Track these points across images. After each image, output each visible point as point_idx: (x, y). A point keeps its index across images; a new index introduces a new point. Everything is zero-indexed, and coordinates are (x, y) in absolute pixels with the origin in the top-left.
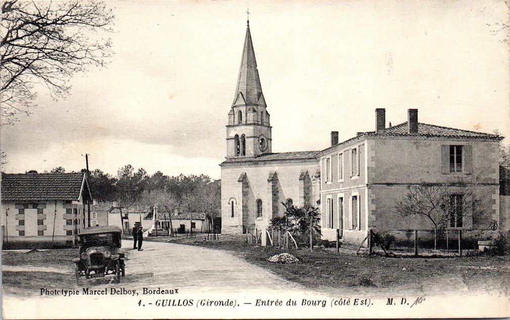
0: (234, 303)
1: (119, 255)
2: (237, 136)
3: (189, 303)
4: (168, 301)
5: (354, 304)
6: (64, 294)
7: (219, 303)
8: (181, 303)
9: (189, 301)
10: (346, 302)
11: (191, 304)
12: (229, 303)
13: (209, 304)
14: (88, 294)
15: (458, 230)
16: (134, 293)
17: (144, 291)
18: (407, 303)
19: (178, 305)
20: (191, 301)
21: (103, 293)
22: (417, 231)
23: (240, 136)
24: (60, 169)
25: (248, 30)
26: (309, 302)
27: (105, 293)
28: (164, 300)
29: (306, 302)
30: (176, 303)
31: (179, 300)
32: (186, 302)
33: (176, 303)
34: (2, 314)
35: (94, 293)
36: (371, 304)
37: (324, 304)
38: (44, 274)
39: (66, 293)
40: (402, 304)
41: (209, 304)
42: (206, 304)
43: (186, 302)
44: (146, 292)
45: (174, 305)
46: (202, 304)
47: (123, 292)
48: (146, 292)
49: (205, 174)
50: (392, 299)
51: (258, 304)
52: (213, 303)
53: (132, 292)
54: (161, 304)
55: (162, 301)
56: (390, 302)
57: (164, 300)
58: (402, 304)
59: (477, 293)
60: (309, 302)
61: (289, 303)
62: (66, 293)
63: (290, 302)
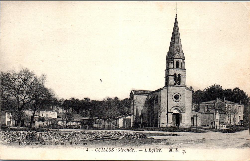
1: (116, 123)
2: (175, 75)
3: (112, 150)
5: (149, 151)
6: (31, 145)
7: (127, 150)
8: (108, 150)
9: (112, 149)
11: (113, 151)
13: (122, 150)
14: (42, 144)
15: (144, 127)
18: (178, 151)
19: (107, 151)
20: (113, 149)
23: (177, 75)
25: (175, 35)
27: (51, 144)
29: (151, 150)
30: (106, 150)
31: (107, 149)
33: (106, 150)
35: (45, 144)
36: (135, 151)
37: (152, 151)
38: (173, 130)
39: (31, 144)
40: (176, 151)
41: (122, 150)
42: (120, 151)
44: (71, 144)
45: (105, 151)
46: (119, 151)
48: (71, 144)
49: (238, 87)
50: (172, 149)
51: (150, 151)
52: (124, 150)
54: (98, 151)
55: (98, 149)
56: (171, 150)
58: (176, 151)
59: (10, 147)
61: (130, 150)
62: (31, 144)
63: (131, 150)
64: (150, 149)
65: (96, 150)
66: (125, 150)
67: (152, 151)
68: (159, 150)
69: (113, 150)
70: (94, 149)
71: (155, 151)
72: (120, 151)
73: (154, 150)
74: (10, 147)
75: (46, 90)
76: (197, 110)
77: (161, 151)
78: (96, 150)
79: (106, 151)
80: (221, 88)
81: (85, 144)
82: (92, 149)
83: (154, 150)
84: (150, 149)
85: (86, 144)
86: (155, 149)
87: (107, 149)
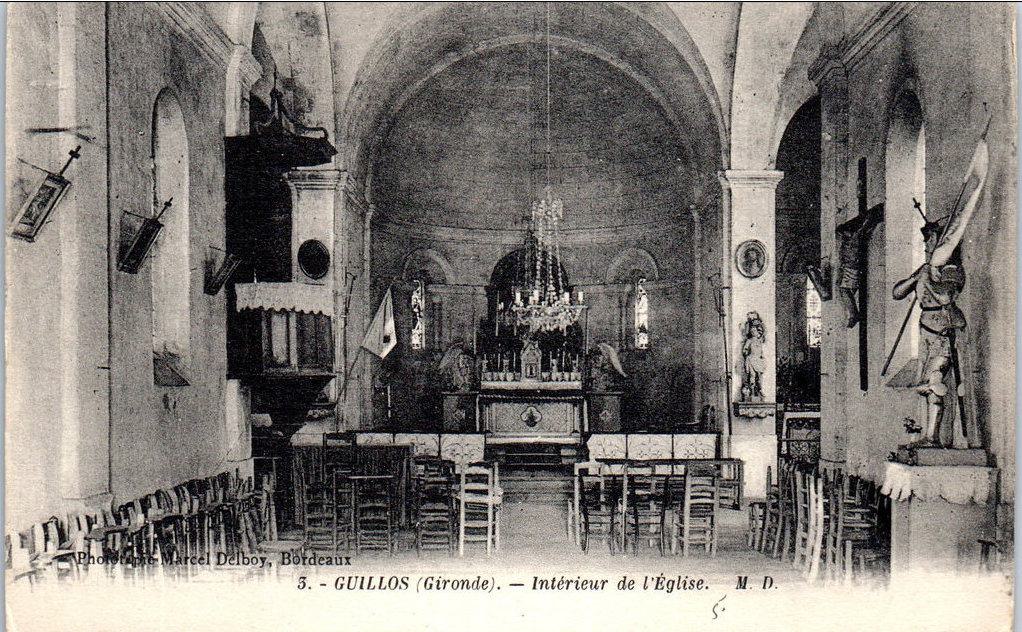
0: (490, 585)
3: (400, 583)
4: (359, 580)
5: (657, 588)
8: (385, 582)
10: (556, 583)
11: (404, 586)
12: (627, 584)
16: (263, 562)
17: (284, 558)
18: (496, 586)
20: (405, 580)
21: (201, 562)
22: (109, 368)
24: (886, 589)
26: (456, 583)
28: (350, 578)
29: (665, 583)
30: (376, 582)
31: (382, 578)
32: (394, 580)
33: (376, 582)
34: (5, 623)
37: (670, 587)
40: (764, 587)
41: (441, 585)
43: (394, 580)
45: (372, 587)
47: (241, 562)
48: (286, 561)
51: (660, 587)
52: (449, 585)
53: (260, 561)
54: (345, 587)
55: (347, 579)
57: (350, 578)
60: (456, 583)
64: (659, 578)
65: (339, 586)
66: (456, 584)
67: (670, 587)
68: (695, 584)
69: (406, 584)
70: (526, 576)
71: (681, 585)
72: (345, 587)
73: (676, 583)
74: (600, 565)
75: (288, 209)
76: (829, 298)
77: (704, 585)
78: (339, 586)
79: (378, 585)
80: (242, 385)
81: (344, 561)
82: (323, 578)
83: (676, 583)
84: (659, 578)
85: (347, 559)
86: (682, 580)
87: (382, 578)
